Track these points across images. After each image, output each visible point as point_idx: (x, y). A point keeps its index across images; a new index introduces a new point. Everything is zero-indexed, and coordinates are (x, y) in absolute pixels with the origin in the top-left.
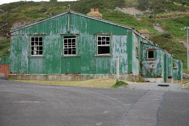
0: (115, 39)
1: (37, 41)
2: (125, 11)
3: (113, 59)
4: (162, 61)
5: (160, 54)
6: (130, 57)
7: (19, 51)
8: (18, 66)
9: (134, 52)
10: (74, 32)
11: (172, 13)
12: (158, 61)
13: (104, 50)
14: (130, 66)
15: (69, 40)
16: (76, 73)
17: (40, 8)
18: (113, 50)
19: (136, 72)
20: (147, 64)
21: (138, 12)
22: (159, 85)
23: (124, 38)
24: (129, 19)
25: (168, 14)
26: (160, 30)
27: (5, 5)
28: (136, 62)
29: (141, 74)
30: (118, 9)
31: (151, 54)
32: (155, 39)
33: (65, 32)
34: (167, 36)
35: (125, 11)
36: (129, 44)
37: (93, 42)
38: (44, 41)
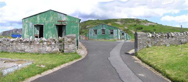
0: (114, 30)
1: (96, 31)
2: (117, 23)
3: (114, 35)
4: (126, 36)
5: (125, 34)
6: (118, 35)
7: (91, 33)
8: (91, 37)
9: (119, 33)
10: (104, 29)
11: (129, 24)
12: (124, 36)
13: (112, 33)
14: (118, 37)
15: (103, 30)
16: (105, 39)
17: (94, 22)
18: (114, 33)
19: (119, 38)
20: (122, 37)
21: (120, 23)
22: (125, 53)
23: (117, 30)
24: (118, 25)
25: (128, 24)
26: (126, 28)
27: (84, 21)
28: (119, 36)
29: (121, 38)
30: (115, 22)
31: (123, 34)
32: (125, 30)
33: (102, 29)
34: (128, 29)
35: (117, 23)
36: (118, 32)
37: (109, 31)
38: (97, 31)
